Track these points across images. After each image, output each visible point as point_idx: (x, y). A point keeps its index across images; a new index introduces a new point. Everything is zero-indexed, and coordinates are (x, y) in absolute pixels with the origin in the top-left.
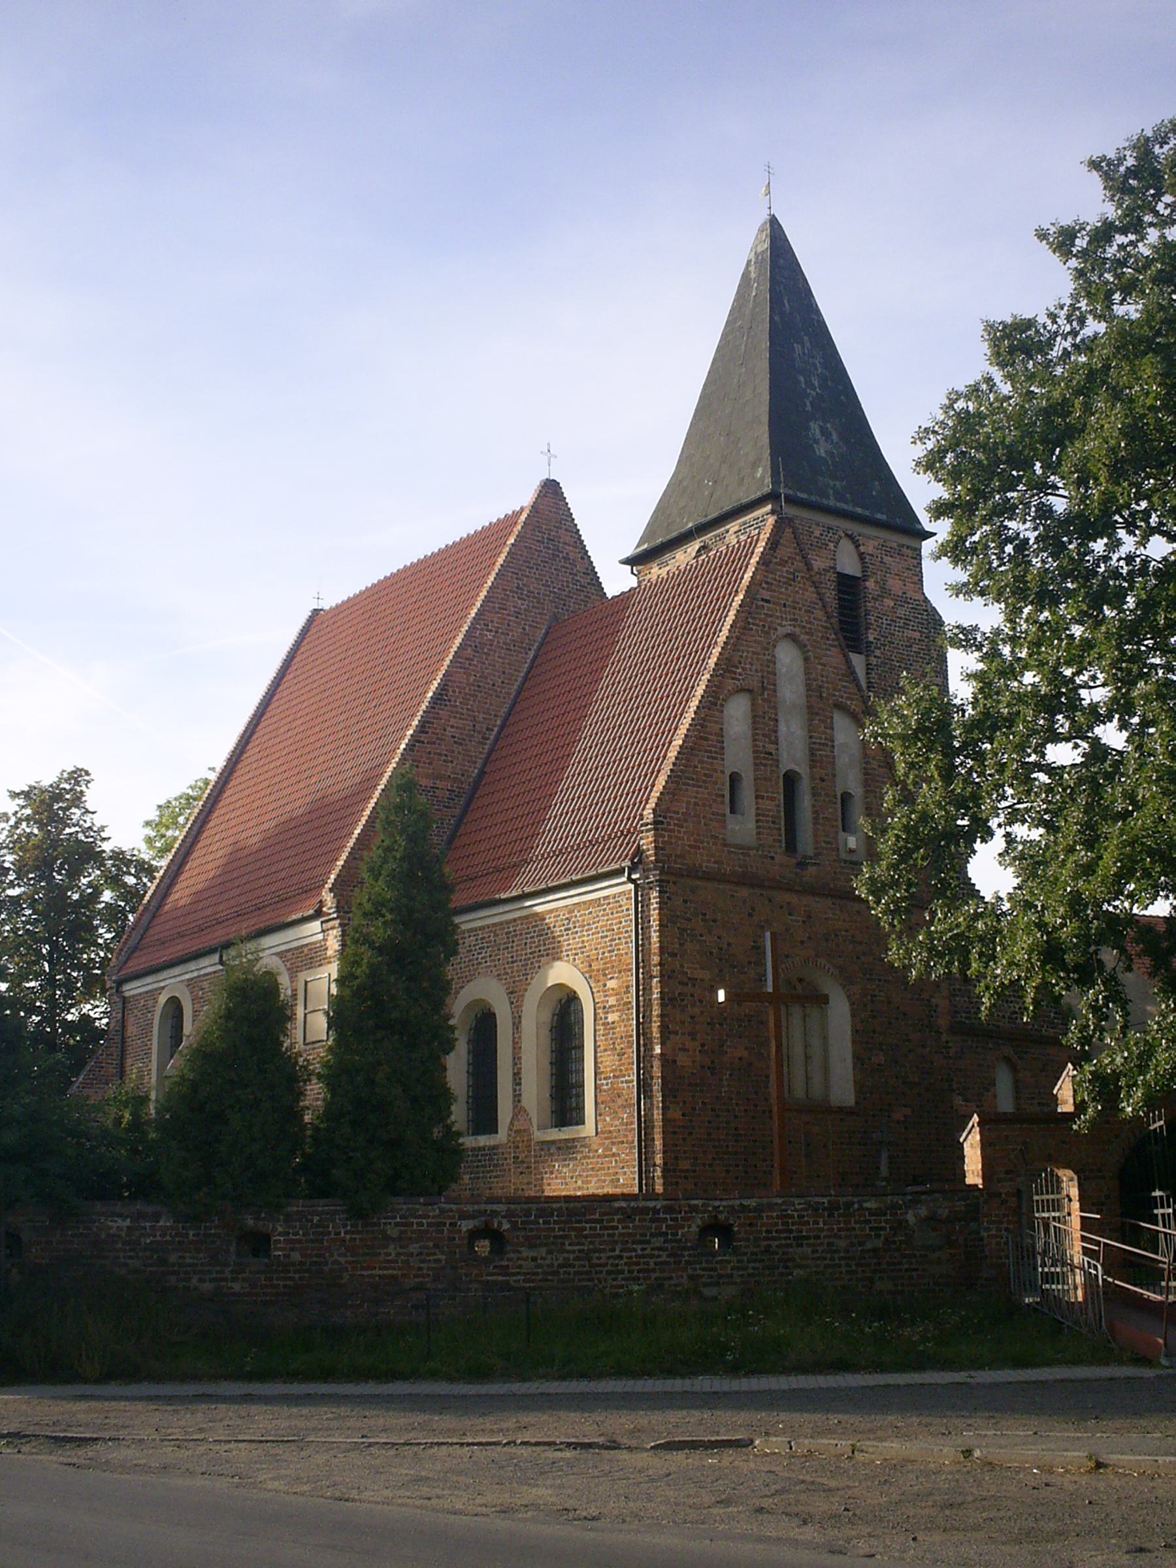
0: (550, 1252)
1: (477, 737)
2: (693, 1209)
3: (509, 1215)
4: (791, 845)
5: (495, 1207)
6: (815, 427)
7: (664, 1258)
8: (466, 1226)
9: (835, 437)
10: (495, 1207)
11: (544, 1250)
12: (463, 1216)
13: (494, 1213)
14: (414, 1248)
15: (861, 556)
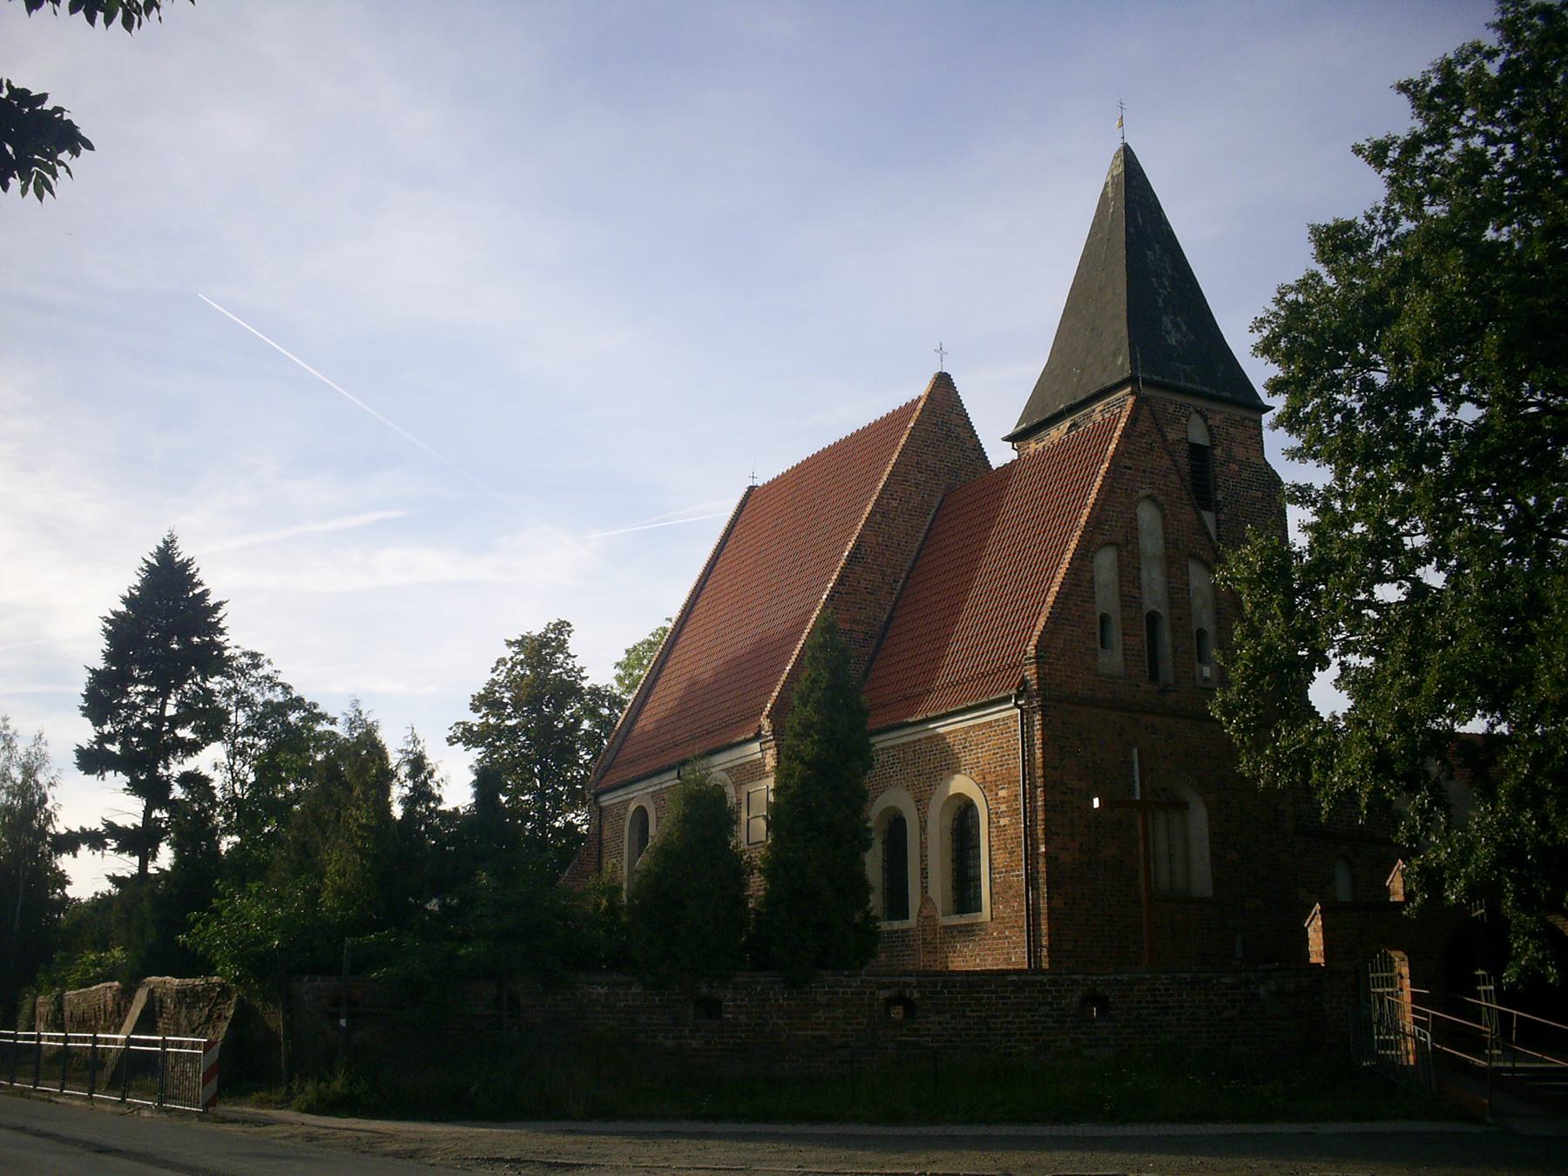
0: (953, 1017)
2: (1075, 982)
4: (1154, 675)
5: (908, 979)
6: (1166, 320)
7: (1050, 1024)
8: (883, 994)
9: (1184, 329)
10: (908, 979)
11: (948, 1016)
12: (881, 986)
13: (907, 985)
14: (840, 1013)
15: (1210, 429)
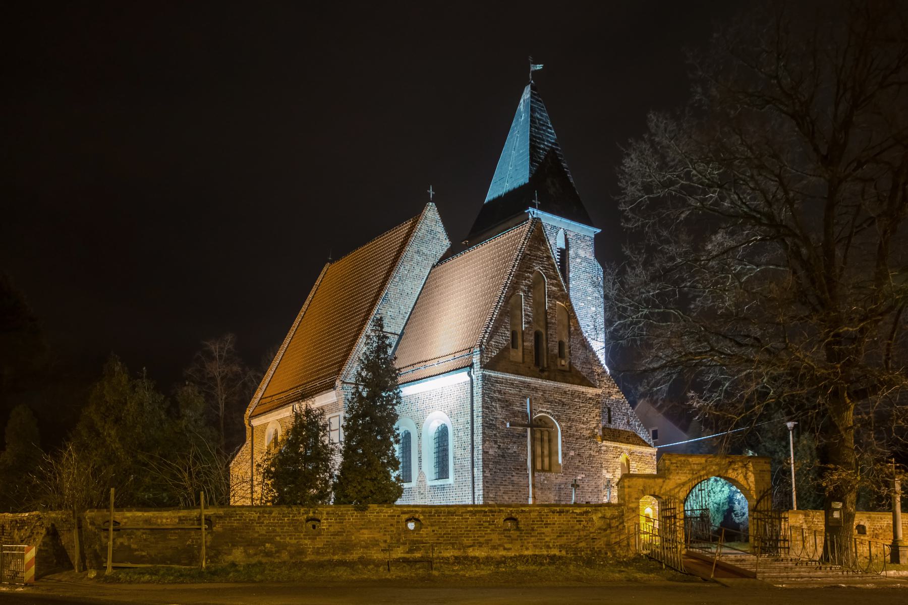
1: (401, 316)
3: (423, 513)
10: (417, 509)
12: (404, 513)
13: (416, 512)
